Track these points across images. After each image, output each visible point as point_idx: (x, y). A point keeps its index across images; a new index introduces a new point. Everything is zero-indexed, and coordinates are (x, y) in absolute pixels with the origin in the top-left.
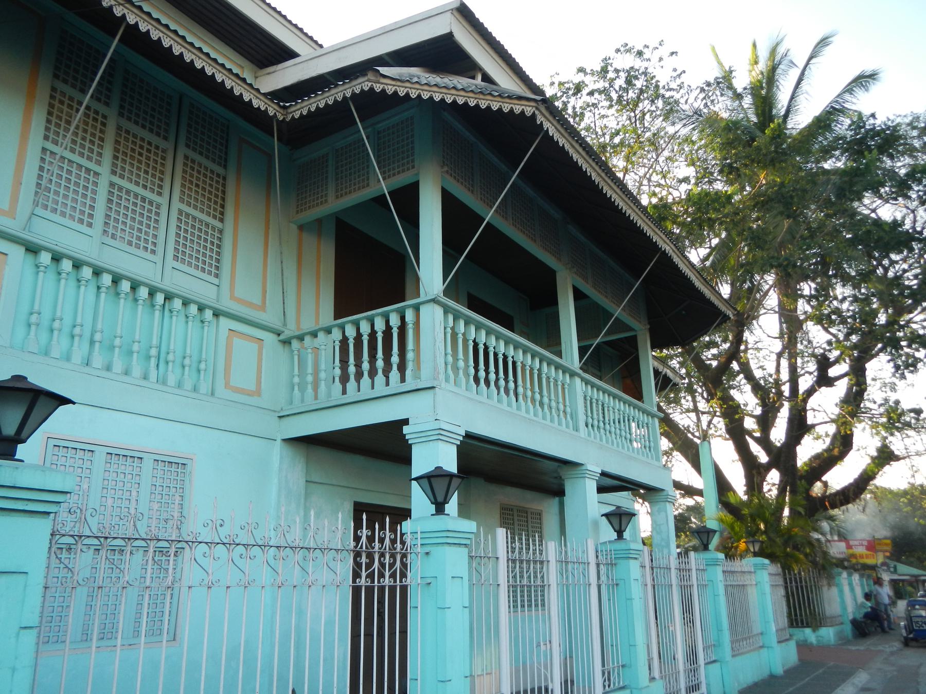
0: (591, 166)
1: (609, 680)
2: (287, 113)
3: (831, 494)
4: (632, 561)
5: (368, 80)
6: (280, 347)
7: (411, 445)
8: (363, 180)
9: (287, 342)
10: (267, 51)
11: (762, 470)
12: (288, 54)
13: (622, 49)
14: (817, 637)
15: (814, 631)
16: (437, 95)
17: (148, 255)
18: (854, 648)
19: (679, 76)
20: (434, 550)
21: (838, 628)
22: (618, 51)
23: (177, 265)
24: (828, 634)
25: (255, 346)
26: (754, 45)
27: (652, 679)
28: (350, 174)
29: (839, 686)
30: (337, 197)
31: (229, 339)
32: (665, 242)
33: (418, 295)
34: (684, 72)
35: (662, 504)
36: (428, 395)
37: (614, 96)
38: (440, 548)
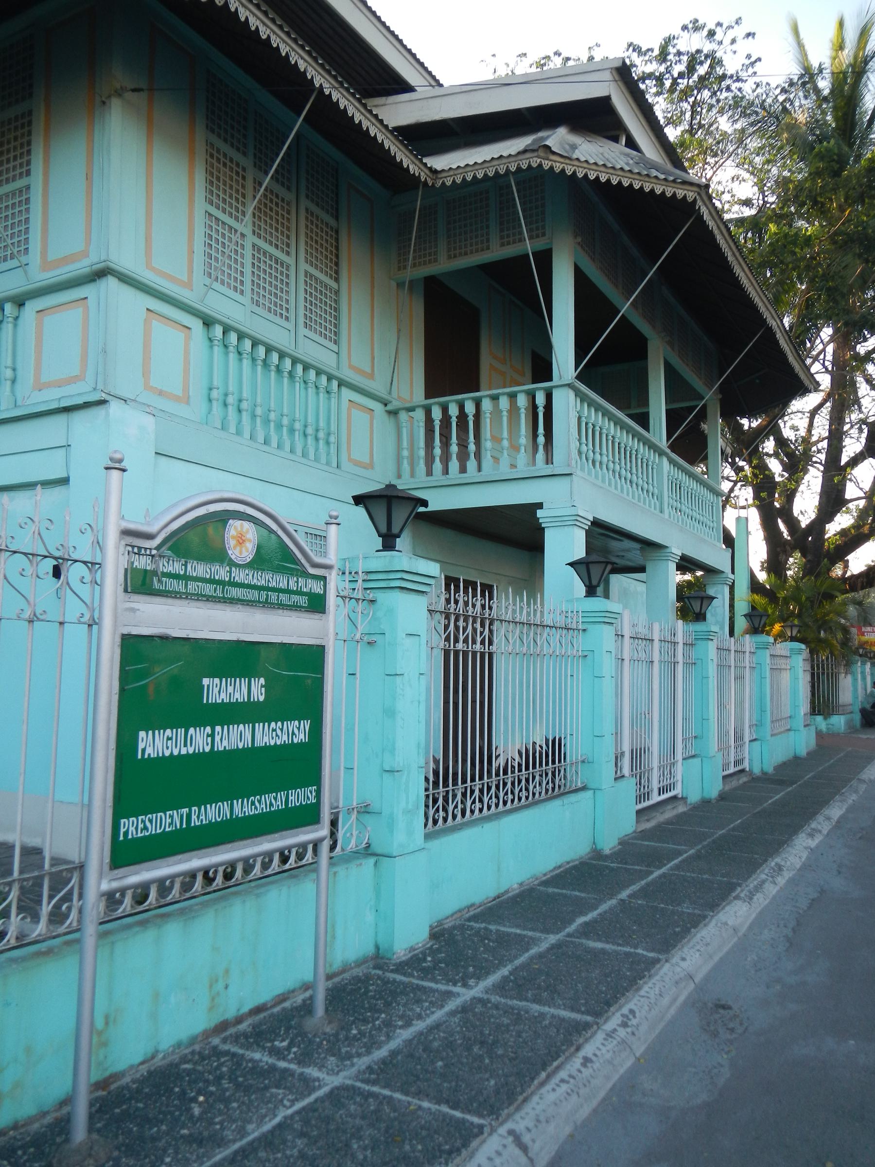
0: (729, 246)
1: (553, 782)
2: (437, 178)
3: (853, 576)
4: (710, 642)
5: (538, 157)
6: (385, 417)
7: (543, 529)
8: (482, 242)
9: (393, 413)
10: (379, 78)
11: (788, 548)
12: (402, 87)
13: (690, 26)
14: (827, 724)
15: (825, 719)
16: (604, 175)
17: (283, 322)
18: (865, 737)
19: (752, 64)
20: (380, 596)
21: (848, 716)
22: (685, 28)
23: (307, 332)
24: (838, 722)
25: (366, 417)
26: (841, 24)
27: (619, 778)
28: (466, 233)
29: (866, 767)
30: (449, 257)
31: (349, 410)
32: (773, 317)
33: (551, 379)
34: (759, 59)
35: (720, 586)
36: (565, 481)
37: (668, 83)
38: (598, 626)
